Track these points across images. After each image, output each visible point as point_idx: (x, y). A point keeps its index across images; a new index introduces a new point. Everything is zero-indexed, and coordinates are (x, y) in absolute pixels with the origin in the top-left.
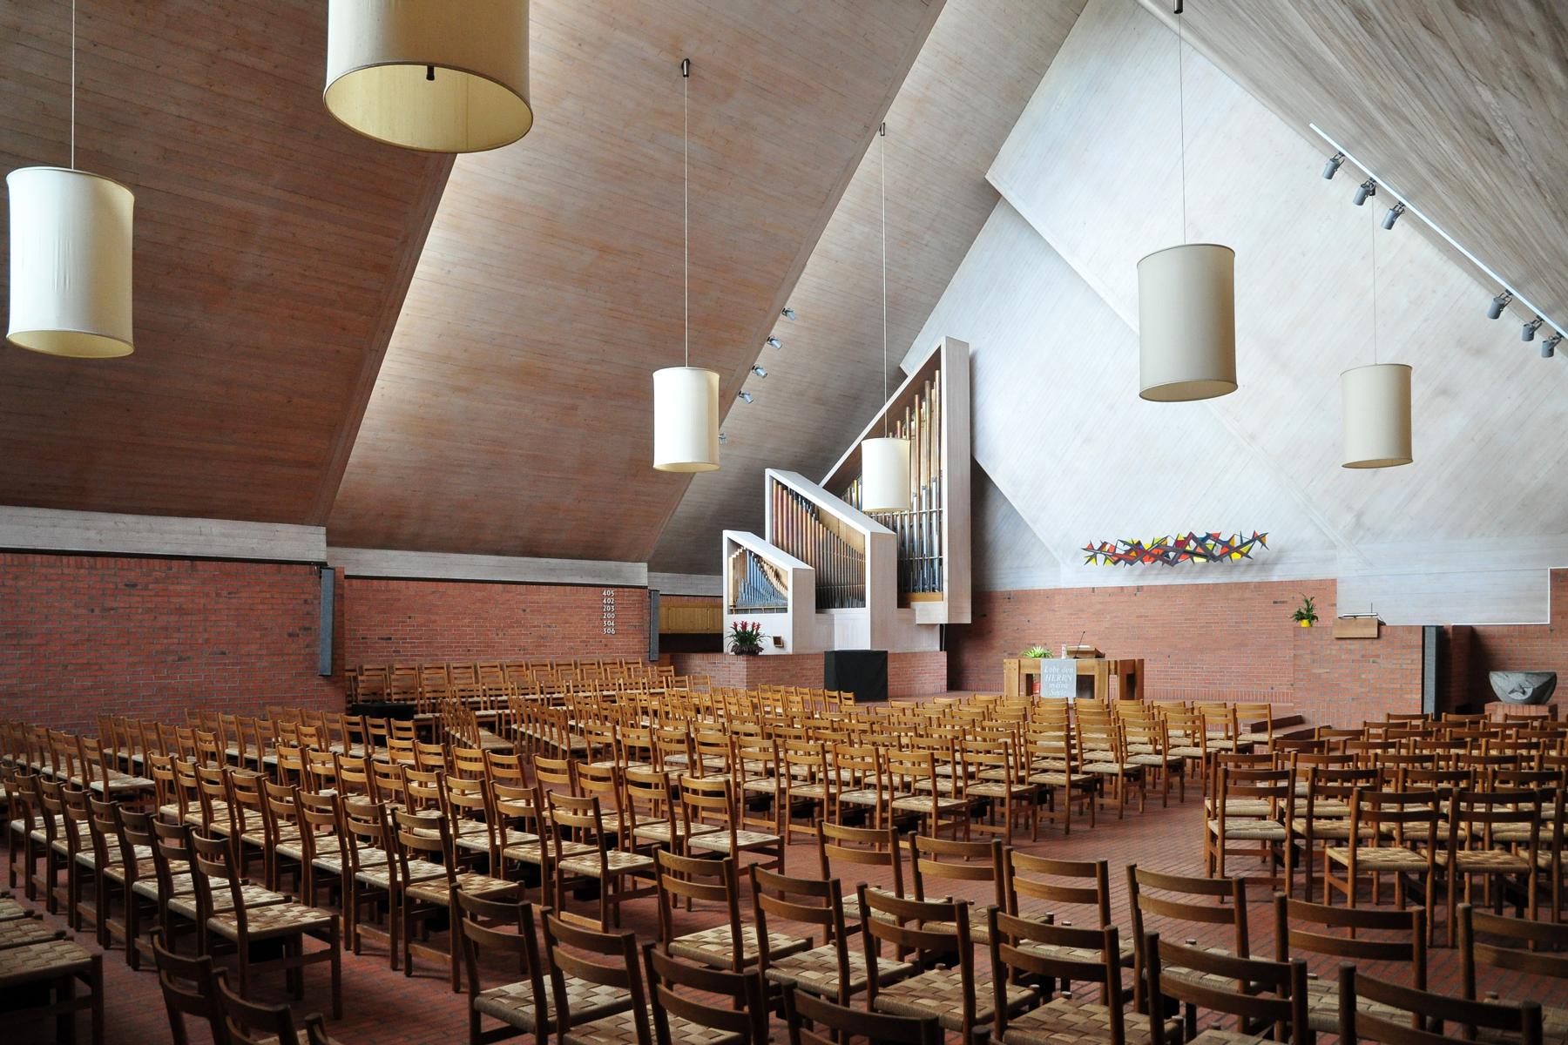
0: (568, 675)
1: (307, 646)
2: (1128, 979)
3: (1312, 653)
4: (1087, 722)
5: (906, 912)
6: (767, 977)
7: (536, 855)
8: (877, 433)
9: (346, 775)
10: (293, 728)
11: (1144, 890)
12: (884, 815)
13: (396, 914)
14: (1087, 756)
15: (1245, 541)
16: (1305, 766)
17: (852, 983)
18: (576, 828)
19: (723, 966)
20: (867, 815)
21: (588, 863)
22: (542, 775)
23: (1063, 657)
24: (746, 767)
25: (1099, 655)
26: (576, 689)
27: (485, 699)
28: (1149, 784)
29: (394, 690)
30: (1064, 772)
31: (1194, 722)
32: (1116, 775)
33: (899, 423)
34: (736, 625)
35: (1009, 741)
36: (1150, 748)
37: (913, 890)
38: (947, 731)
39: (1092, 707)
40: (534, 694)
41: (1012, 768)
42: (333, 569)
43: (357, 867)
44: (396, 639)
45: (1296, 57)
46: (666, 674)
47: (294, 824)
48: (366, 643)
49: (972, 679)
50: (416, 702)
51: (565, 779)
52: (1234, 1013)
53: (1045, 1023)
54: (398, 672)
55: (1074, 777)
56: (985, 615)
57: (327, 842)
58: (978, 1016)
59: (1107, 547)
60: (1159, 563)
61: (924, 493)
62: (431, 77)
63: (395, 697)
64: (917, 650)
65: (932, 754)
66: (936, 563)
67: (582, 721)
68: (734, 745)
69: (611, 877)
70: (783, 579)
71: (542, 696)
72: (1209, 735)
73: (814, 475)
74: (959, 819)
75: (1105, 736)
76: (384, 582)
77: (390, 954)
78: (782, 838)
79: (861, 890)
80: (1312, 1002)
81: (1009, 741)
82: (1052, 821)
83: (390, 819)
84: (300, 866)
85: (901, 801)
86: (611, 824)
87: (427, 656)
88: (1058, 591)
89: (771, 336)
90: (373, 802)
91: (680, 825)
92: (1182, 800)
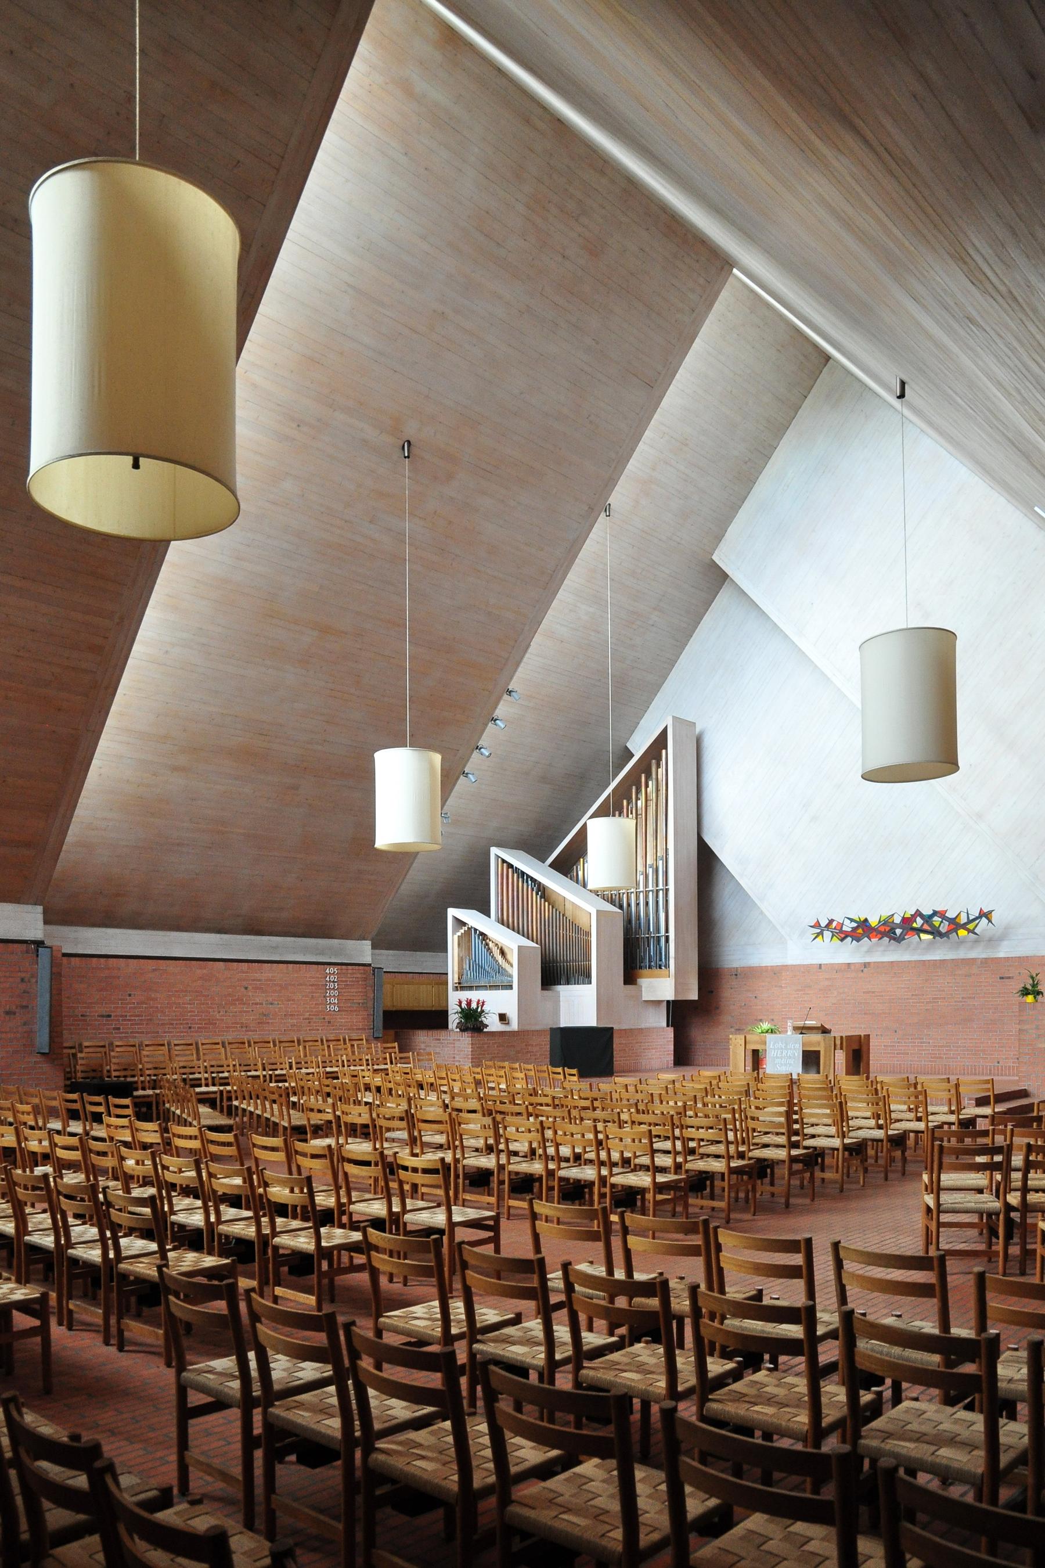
0: (291, 1051)
1: (25, 1024)
2: (829, 1352)
3: (1037, 1028)
4: (809, 1098)
5: (614, 1289)
6: (474, 1351)
7: (251, 1232)
8: (603, 812)
9: (61, 1153)
10: (10, 1106)
11: (848, 1266)
12: (603, 1190)
13: (108, 1290)
14: (809, 1131)
15: (971, 917)
16: (1020, 1141)
17: (558, 1357)
18: (292, 1206)
19: (431, 1341)
20: (586, 1190)
21: (302, 1240)
22: (258, 1153)
23: (789, 1033)
24: (465, 1143)
25: (825, 1031)
26: (299, 1066)
27: (206, 1075)
28: (871, 1157)
29: (113, 1067)
30: (784, 1146)
31: (917, 1097)
32: (837, 1149)
33: (625, 802)
34: (460, 1002)
35: (729, 1116)
36: (872, 1122)
37: (623, 1266)
38: (670, 1107)
39: (815, 1082)
40: (256, 1070)
41: (732, 1143)
42: (51, 948)
43: (70, 1245)
44: (116, 1016)
45: (1013, 444)
46: (390, 1050)
47: (8, 1202)
48: (86, 1021)
49: (699, 1056)
50: (136, 1079)
51: (281, 1156)
52: (935, 1387)
53: (745, 1395)
54: (118, 1049)
55: (794, 1152)
56: (712, 992)
57: (39, 1219)
58: (680, 1389)
59: (834, 924)
60: (886, 939)
61: (650, 871)
62: (136, 465)
63: (114, 1074)
64: (643, 1026)
65: (650, 1131)
66: (663, 940)
67: (305, 1098)
68: (453, 1125)
69: (324, 1253)
70: (509, 957)
71: (264, 1073)
72: (930, 1109)
73: (539, 852)
74: (678, 1194)
75: (828, 1111)
76: (102, 960)
77: (102, 1329)
78: (498, 1214)
79: (566, 1267)
80: (1001, 1371)
81: (729, 1116)
82: (773, 1195)
83: (101, 1196)
84: (13, 1243)
85: (619, 1176)
86: (325, 1200)
87: (147, 1033)
88: (785, 968)
89: (495, 716)
90: (88, 1179)
91: (396, 1201)
92: (904, 1174)
